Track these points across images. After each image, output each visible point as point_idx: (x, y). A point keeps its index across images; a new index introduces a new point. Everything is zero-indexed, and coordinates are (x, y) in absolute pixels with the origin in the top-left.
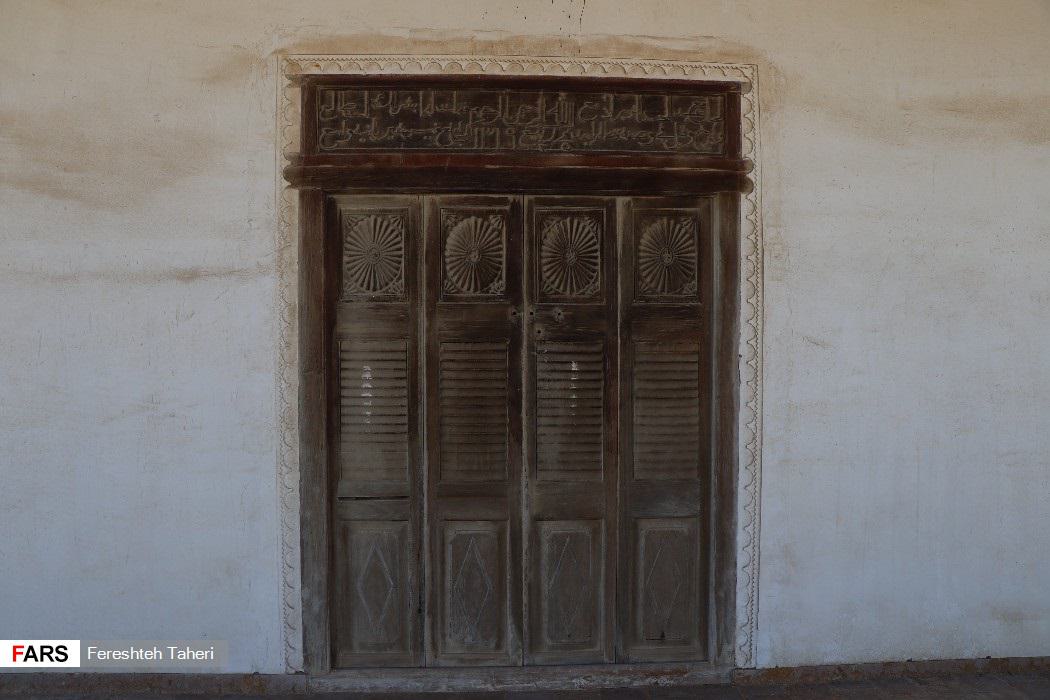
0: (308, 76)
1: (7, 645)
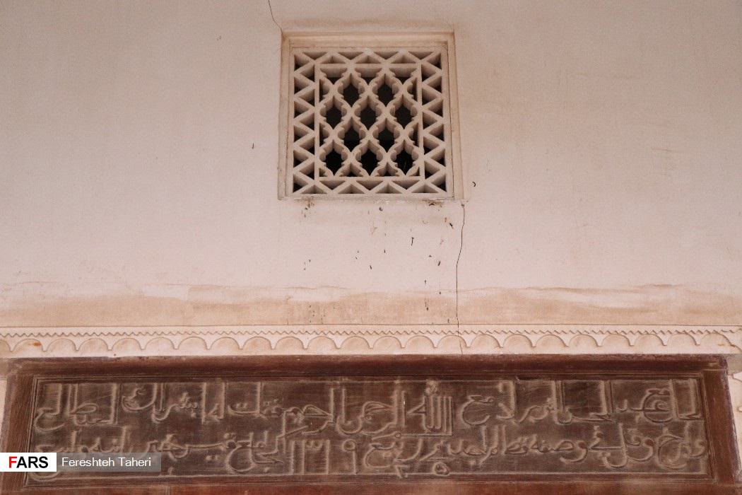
0: (20, 361)
1: (6, 456)
